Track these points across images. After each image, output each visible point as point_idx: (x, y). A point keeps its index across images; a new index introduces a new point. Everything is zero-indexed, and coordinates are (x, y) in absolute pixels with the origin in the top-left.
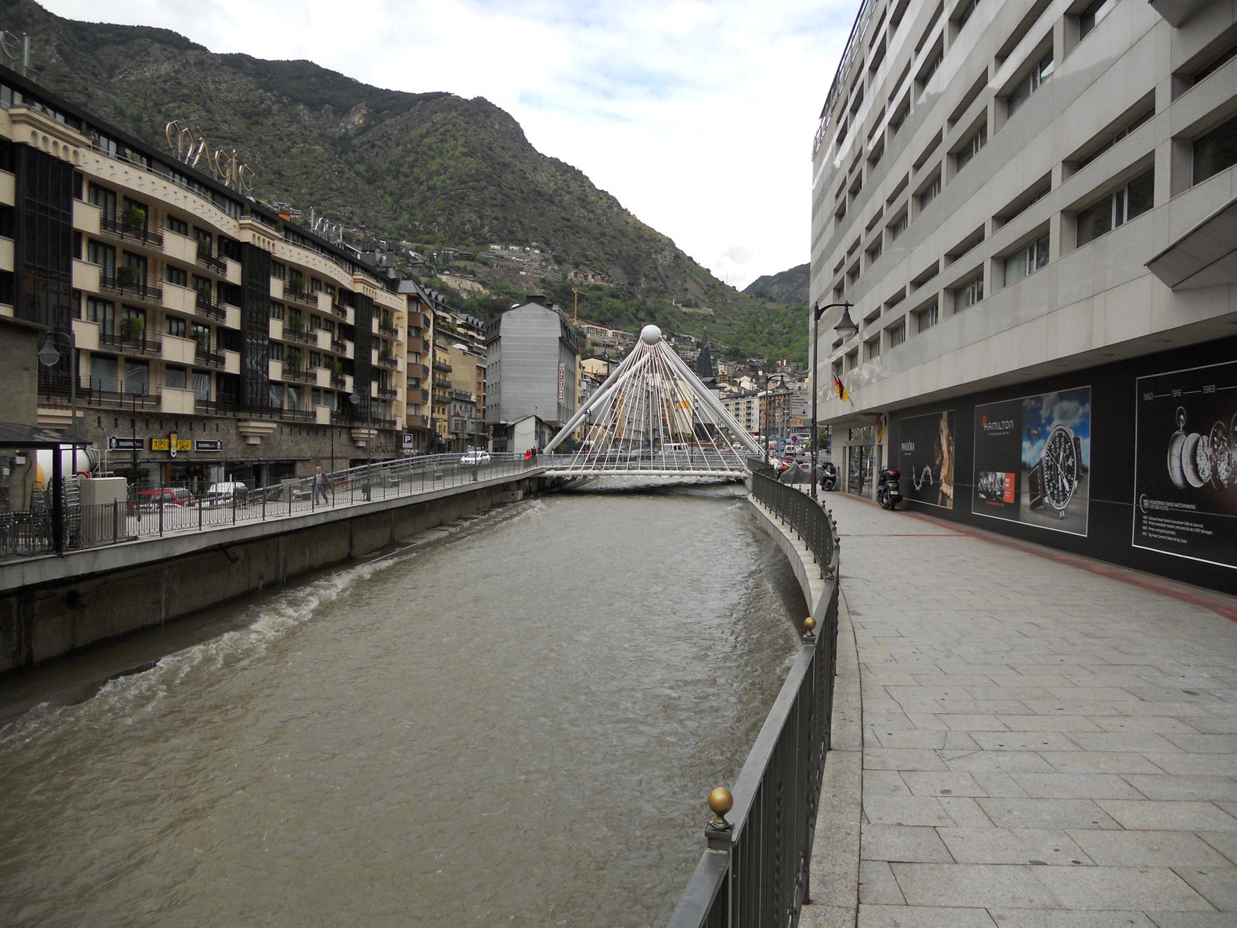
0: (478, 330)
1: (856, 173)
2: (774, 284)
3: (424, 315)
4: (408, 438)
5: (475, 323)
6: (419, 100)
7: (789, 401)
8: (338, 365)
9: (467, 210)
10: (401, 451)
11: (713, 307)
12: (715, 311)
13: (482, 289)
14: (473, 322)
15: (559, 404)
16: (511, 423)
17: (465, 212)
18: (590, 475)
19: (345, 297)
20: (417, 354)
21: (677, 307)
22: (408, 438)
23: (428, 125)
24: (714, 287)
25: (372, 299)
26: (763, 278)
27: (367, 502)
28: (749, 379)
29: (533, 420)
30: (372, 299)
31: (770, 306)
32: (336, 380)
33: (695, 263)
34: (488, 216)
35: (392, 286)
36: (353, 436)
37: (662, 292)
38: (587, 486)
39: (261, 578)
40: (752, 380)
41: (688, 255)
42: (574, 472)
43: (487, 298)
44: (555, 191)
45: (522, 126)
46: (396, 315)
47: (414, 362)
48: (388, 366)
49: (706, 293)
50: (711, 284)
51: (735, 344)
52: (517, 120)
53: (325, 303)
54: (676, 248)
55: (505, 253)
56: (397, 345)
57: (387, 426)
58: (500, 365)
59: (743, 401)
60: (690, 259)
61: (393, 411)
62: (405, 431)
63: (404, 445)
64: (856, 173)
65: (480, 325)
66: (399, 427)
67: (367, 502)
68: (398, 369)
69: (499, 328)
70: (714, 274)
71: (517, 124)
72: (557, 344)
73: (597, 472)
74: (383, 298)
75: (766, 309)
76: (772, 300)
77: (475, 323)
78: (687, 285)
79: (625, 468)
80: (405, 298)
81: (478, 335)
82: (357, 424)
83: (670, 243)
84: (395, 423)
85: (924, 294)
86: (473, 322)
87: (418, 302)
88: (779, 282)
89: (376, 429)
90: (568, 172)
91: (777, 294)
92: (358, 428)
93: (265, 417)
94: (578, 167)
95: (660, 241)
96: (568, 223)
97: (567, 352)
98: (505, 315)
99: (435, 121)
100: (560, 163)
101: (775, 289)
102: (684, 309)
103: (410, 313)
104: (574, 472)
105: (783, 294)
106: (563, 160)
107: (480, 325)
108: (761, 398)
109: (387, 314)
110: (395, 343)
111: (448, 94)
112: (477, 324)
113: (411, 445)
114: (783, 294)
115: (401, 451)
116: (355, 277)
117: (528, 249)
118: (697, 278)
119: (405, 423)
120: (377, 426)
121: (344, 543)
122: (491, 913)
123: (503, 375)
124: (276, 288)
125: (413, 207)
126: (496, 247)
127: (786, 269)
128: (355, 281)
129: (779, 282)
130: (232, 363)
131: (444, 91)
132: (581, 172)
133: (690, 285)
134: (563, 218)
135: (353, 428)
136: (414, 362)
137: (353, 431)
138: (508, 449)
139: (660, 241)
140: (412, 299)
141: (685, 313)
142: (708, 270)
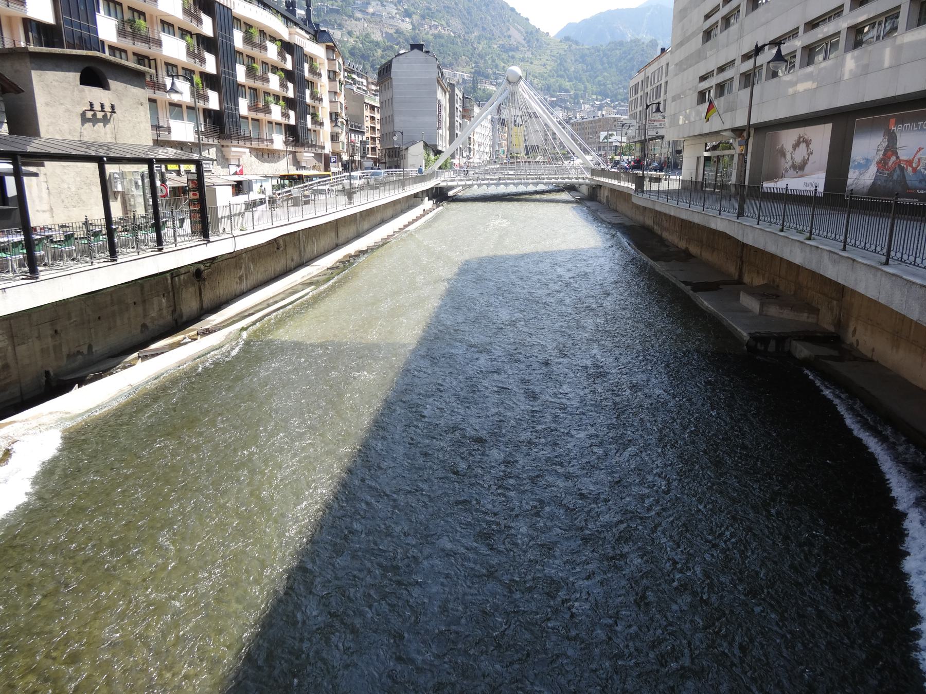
8: (197, 79)
19: (287, 47)
24: (531, 33)
29: (422, 144)
32: (198, 94)
33: (517, 14)
37: (490, 39)
39: (292, 260)
41: (511, 6)
48: (317, 102)
49: (524, 40)
50: (530, 31)
53: (272, 52)
57: (319, 151)
60: (513, 10)
69: (390, 70)
70: (532, 22)
84: (323, 147)
85: (726, 75)
93: (242, 143)
109: (311, 59)
121: (333, 235)
122: (60, 520)
123: (395, 109)
124: (238, 38)
130: (213, 101)
133: (513, 32)
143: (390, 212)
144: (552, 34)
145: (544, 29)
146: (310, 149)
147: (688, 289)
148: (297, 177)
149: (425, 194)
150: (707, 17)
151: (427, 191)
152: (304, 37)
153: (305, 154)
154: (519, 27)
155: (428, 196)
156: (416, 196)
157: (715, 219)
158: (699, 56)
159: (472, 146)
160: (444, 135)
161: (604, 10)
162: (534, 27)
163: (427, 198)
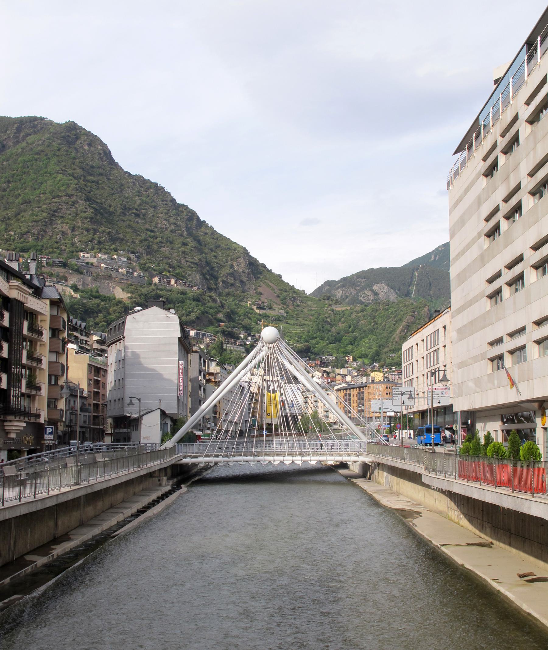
0: (81, 331)
1: (513, 201)
2: (338, 288)
3: (62, 317)
4: (49, 430)
5: (78, 325)
6: (15, 123)
7: (363, 393)
9: (59, 222)
10: (43, 442)
11: (285, 309)
12: (287, 313)
13: (73, 293)
14: (76, 324)
15: (178, 397)
16: (135, 416)
17: (57, 224)
18: (220, 462)
20: (57, 353)
21: (252, 309)
22: (49, 430)
23: (24, 144)
25: (23, 304)
26: (328, 283)
27: (78, 487)
28: (320, 374)
29: (158, 413)
30: (22, 304)
31: (338, 308)
34: (79, 227)
35: (38, 292)
36: (6, 428)
38: (208, 474)
40: (323, 375)
42: (207, 459)
43: (79, 302)
44: (140, 205)
45: (110, 147)
46: (40, 318)
47: (55, 361)
49: (278, 296)
51: (306, 341)
52: (105, 142)
54: (250, 256)
55: (94, 261)
56: (40, 345)
57: (33, 420)
58: (124, 364)
59: (354, 392)
61: (36, 406)
62: (46, 423)
63: (46, 437)
64: (513, 201)
65: (83, 327)
66: (42, 420)
67: (78, 487)
68: (43, 367)
70: (285, 279)
71: (104, 146)
72: (177, 341)
73: (226, 459)
74: (32, 303)
75: (333, 311)
76: (337, 302)
77: (78, 325)
78: (260, 290)
79: (251, 455)
80: (48, 302)
81: (82, 335)
82: (9, 418)
83: (246, 252)
84: (38, 416)
86: (76, 324)
87: (58, 306)
88: (343, 286)
89: (25, 422)
90: (151, 188)
91: (341, 296)
92: (10, 421)
94: (161, 183)
95: (235, 250)
96: (152, 234)
97: (183, 351)
98: (129, 318)
99: (29, 142)
100: (144, 180)
101: (339, 293)
102: (258, 311)
103: (51, 316)
104: (207, 459)
105: (347, 297)
106: (146, 178)
107: (83, 327)
108: (337, 390)
109: (32, 315)
110: (39, 343)
111: (42, 119)
112: (80, 326)
113: (52, 437)
114: (347, 297)
115: (43, 442)
116: (11, 284)
117: (115, 257)
118: (270, 284)
119: (46, 417)
120: (26, 419)
125: (9, 219)
126: (86, 255)
127: (348, 274)
128: (11, 288)
129: (343, 286)
131: (39, 116)
132: (163, 188)
134: (148, 230)
135: (6, 421)
136: (55, 361)
137: (6, 424)
138: (132, 440)
139: (235, 250)
140: (56, 303)
141: (260, 315)
142: (280, 276)
143: (120, 495)
144: (309, 291)
145: (299, 287)
146: (22, 418)
147: (439, 546)
148: (172, 492)
149: (162, 474)
150: (490, 281)
151: (165, 469)
152: (25, 293)
153: (16, 424)
154: (270, 284)
155: (166, 475)
156: (151, 475)
157: (528, 502)
158: (483, 260)
159: (217, 416)
160: (185, 402)
161: (365, 269)
162: (288, 284)
163: (165, 478)
